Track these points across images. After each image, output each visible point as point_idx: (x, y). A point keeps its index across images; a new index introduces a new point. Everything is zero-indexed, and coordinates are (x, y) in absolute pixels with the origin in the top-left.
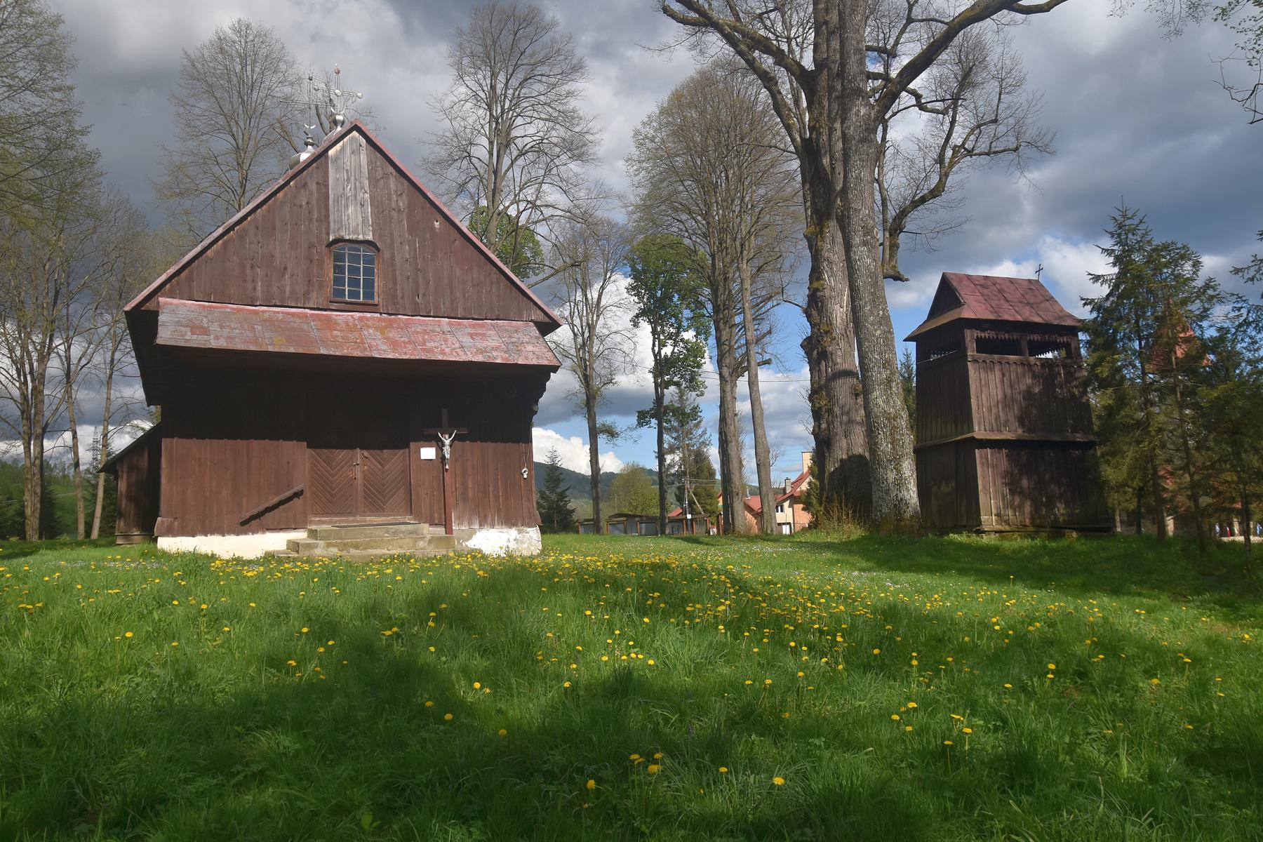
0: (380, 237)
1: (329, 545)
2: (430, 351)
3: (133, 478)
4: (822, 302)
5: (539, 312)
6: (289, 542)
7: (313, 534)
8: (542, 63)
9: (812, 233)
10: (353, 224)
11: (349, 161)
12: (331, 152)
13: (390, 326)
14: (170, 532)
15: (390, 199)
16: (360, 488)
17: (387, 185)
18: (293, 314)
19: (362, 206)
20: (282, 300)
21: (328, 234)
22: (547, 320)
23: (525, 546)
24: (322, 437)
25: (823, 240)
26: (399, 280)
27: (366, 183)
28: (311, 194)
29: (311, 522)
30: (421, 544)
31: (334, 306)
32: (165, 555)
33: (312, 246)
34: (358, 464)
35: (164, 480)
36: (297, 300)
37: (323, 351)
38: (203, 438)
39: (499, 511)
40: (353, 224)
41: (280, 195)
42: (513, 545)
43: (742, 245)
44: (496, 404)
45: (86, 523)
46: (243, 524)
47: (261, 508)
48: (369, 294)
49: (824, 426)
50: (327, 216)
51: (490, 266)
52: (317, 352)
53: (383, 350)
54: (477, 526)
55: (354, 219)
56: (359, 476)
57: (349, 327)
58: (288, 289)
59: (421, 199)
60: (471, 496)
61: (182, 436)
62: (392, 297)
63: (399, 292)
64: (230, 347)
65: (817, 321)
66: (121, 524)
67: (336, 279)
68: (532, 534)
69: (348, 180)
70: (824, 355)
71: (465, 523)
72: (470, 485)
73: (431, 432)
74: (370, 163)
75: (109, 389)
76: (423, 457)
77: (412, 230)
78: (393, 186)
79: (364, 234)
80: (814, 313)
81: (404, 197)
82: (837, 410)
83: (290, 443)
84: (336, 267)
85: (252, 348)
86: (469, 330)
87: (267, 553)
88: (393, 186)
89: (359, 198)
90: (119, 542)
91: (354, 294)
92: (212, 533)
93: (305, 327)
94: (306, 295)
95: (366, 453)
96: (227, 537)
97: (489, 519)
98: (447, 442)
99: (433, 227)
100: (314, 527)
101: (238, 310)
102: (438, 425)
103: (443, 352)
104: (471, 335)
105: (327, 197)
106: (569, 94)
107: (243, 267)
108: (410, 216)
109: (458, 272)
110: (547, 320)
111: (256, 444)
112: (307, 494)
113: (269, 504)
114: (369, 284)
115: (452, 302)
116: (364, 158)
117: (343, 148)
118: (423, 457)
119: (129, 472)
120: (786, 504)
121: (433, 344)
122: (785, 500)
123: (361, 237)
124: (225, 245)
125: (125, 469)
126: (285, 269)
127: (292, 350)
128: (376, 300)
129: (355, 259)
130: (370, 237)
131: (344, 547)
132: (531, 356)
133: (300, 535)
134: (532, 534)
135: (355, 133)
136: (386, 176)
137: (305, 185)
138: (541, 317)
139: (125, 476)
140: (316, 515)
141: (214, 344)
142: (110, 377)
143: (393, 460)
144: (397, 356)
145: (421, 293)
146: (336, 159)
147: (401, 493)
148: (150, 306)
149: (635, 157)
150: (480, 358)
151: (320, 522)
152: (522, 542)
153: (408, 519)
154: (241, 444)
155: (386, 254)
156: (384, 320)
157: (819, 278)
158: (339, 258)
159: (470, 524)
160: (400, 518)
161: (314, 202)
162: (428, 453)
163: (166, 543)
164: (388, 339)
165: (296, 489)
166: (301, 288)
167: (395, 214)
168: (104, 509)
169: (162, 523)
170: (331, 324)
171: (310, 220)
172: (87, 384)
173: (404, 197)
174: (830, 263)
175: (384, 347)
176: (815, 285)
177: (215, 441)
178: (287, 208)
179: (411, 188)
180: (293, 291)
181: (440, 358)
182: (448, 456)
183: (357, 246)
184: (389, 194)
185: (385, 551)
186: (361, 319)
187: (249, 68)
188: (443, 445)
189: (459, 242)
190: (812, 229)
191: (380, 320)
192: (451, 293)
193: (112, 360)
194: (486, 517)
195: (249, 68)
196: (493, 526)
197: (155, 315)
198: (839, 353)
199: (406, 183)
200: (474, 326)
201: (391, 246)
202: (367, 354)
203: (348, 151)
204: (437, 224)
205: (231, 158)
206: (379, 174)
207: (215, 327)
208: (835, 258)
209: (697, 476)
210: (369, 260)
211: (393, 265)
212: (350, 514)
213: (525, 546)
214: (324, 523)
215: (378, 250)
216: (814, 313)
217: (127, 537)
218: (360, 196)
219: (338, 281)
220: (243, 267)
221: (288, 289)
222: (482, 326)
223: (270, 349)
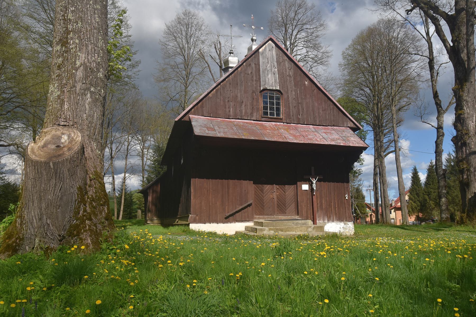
0: (282, 88)
1: (270, 229)
2: (311, 139)
3: (154, 195)
4: (463, 120)
5: (351, 123)
6: (246, 227)
7: (256, 223)
8: (305, 24)
9: (457, 89)
10: (271, 82)
11: (268, 53)
12: (260, 50)
13: (289, 128)
14: (195, 221)
15: (286, 72)
16: (276, 203)
17: (284, 65)
18: (247, 123)
19: (274, 74)
20: (241, 116)
21: (260, 87)
22: (355, 126)
23: (347, 230)
24: (260, 179)
25: (463, 91)
26: (291, 108)
27: (276, 64)
28: (252, 69)
29: (255, 218)
30: (310, 229)
31: (263, 119)
32: (194, 233)
33: (253, 92)
34: (272, 192)
35: (192, 198)
36: (248, 116)
37: (266, 139)
38: (209, 179)
39: (336, 214)
40: (271, 82)
41: (239, 69)
42: (342, 230)
43: (392, 99)
44: (335, 164)
45: (119, 214)
46: (226, 218)
47: (234, 211)
48: (278, 114)
50: (260, 79)
51: (329, 102)
52: (263, 139)
53: (291, 139)
54: (326, 221)
55: (271, 80)
56: (275, 197)
57: (273, 129)
58: (244, 111)
59: (300, 71)
60: (324, 207)
61: (200, 178)
62: (288, 115)
63: (291, 114)
64: (226, 136)
65: (461, 128)
66: (149, 215)
67: (264, 107)
68: (350, 225)
69: (268, 62)
70: (464, 144)
71: (322, 220)
72: (323, 202)
74: (277, 55)
75: (126, 160)
76: (303, 189)
77: (296, 85)
78: (287, 66)
79: (275, 87)
80: (459, 125)
81: (292, 70)
83: (246, 181)
84: (264, 102)
85: (236, 137)
86: (323, 131)
87: (236, 232)
88: (287, 66)
89: (273, 71)
90: (148, 222)
91: (272, 114)
92: (213, 222)
93: (254, 128)
94: (252, 113)
95: (278, 187)
96: (219, 224)
97: (332, 218)
98: (314, 182)
99: (305, 84)
100: (256, 220)
101: (223, 120)
102: (311, 175)
103: (316, 140)
104: (325, 133)
105: (260, 70)
106: (317, 36)
107: (224, 102)
108: (295, 79)
109: (316, 104)
110: (355, 126)
111: (231, 182)
112: (253, 205)
113: (237, 210)
114: (278, 109)
115: (314, 118)
116: (274, 53)
117: (265, 48)
118: (303, 189)
119: (153, 192)
120: (393, 211)
121: (312, 137)
122: (392, 209)
123: (274, 88)
124: (217, 91)
125: (151, 191)
126: (242, 102)
127: (253, 138)
128: (281, 117)
129: (271, 98)
130: (278, 88)
131: (277, 230)
132: (355, 143)
133: (251, 224)
134: (350, 225)
135: (270, 42)
136: (284, 61)
137: (250, 65)
138: (352, 125)
139: (151, 194)
140: (257, 215)
141: (219, 135)
142: (127, 156)
143: (290, 190)
144: (298, 141)
145: (301, 113)
146: (263, 53)
147: (293, 206)
148: (186, 119)
149: (342, 63)
150: (333, 143)
151: (259, 218)
152: (346, 229)
153: (297, 217)
154: (225, 181)
155: (285, 96)
156: (286, 126)
157: (462, 109)
158: (265, 97)
159: (324, 220)
160: (293, 217)
161: (254, 72)
162: (305, 187)
163: (193, 226)
164: (291, 134)
165: (249, 203)
166: (249, 111)
167: (288, 78)
168: (124, 208)
169: (192, 216)
170: (264, 128)
171: (253, 80)
172: (118, 158)
173: (292, 70)
174: (467, 102)
175: (291, 138)
176: (460, 112)
177: (214, 180)
178: (242, 75)
179: (295, 66)
180: (246, 113)
181: (317, 143)
182: (315, 189)
183: (272, 92)
184: (286, 69)
185: (294, 233)
186: (276, 125)
187: (190, 29)
188: (312, 183)
189: (316, 91)
190: (457, 86)
191: (284, 126)
192: (313, 114)
193: (128, 149)
194: (330, 217)
195: (190, 29)
196: (333, 221)
197: (189, 122)
198: (473, 143)
199: (293, 64)
200: (325, 129)
201: (287, 92)
202: (285, 140)
203: (268, 49)
204: (306, 83)
205: (182, 66)
206: (281, 60)
207: (216, 128)
208: (469, 100)
209: (357, 198)
210: (278, 99)
211: (288, 101)
212: (271, 215)
213: (347, 230)
214: (260, 218)
215: (282, 94)
216: (459, 125)
217: (152, 220)
218: (273, 70)
219: (278, 104)
220: (224, 102)
221: (244, 111)
222: (328, 129)
223: (243, 137)
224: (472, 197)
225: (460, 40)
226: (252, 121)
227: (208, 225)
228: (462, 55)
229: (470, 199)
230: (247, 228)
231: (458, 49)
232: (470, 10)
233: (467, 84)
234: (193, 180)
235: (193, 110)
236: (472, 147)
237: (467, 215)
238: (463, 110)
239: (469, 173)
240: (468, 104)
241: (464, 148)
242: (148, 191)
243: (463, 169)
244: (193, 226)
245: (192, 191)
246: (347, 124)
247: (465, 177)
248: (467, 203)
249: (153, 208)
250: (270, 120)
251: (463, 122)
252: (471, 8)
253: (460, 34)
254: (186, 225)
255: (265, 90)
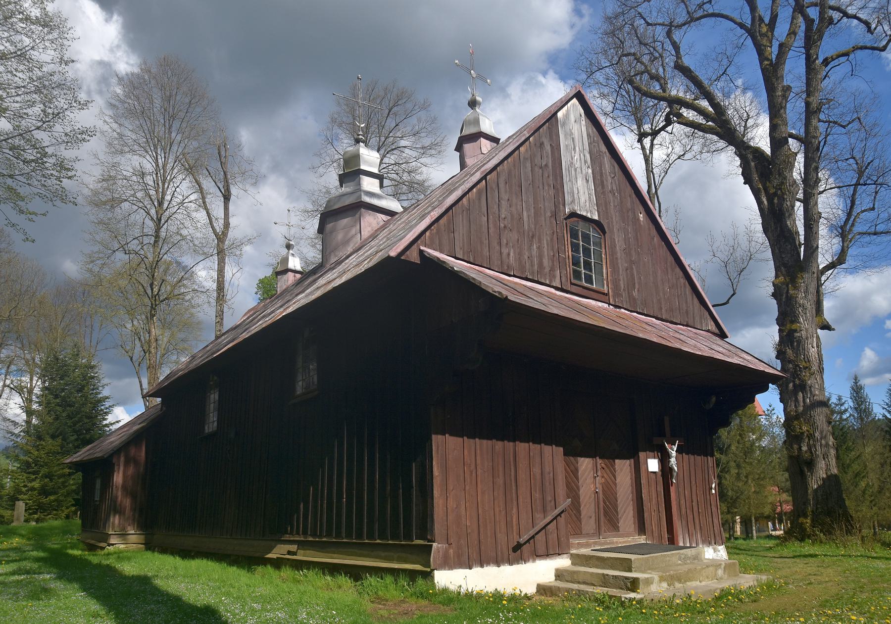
3: (131, 470)
4: (799, 342)
6: (557, 570)
14: (448, 564)
25: (796, 288)
32: (450, 598)
35: (436, 493)
37: (641, 335)
49: (796, 446)
51: (678, 270)
73: (656, 441)
80: (789, 351)
82: (817, 434)
89: (584, 172)
92: (488, 564)
96: (502, 567)
102: (662, 434)
111: (522, 447)
117: (568, 111)
119: (127, 463)
125: (122, 459)
130: (596, 217)
133: (564, 562)
139: (122, 468)
157: (795, 320)
163: (447, 579)
169: (438, 549)
188: (669, 456)
190: (781, 279)
217: (123, 535)
224: (819, 487)
225: (783, 194)
226: (553, 290)
227: (491, 571)
228: (788, 223)
229: (816, 491)
230: (560, 575)
231: (781, 210)
232: (813, 140)
233: (806, 276)
234: (437, 440)
235: (428, 233)
236: (817, 392)
237: (813, 521)
238: (799, 323)
239: (811, 442)
240: (806, 314)
241: (801, 394)
242: (114, 461)
243: (802, 433)
244: (447, 579)
245: (436, 472)
246: (707, 325)
247: (804, 448)
248: (810, 497)
249: (128, 503)
250: (585, 292)
251: (798, 345)
252: (815, 137)
253: (782, 183)
254: (412, 575)
255: (573, 215)
